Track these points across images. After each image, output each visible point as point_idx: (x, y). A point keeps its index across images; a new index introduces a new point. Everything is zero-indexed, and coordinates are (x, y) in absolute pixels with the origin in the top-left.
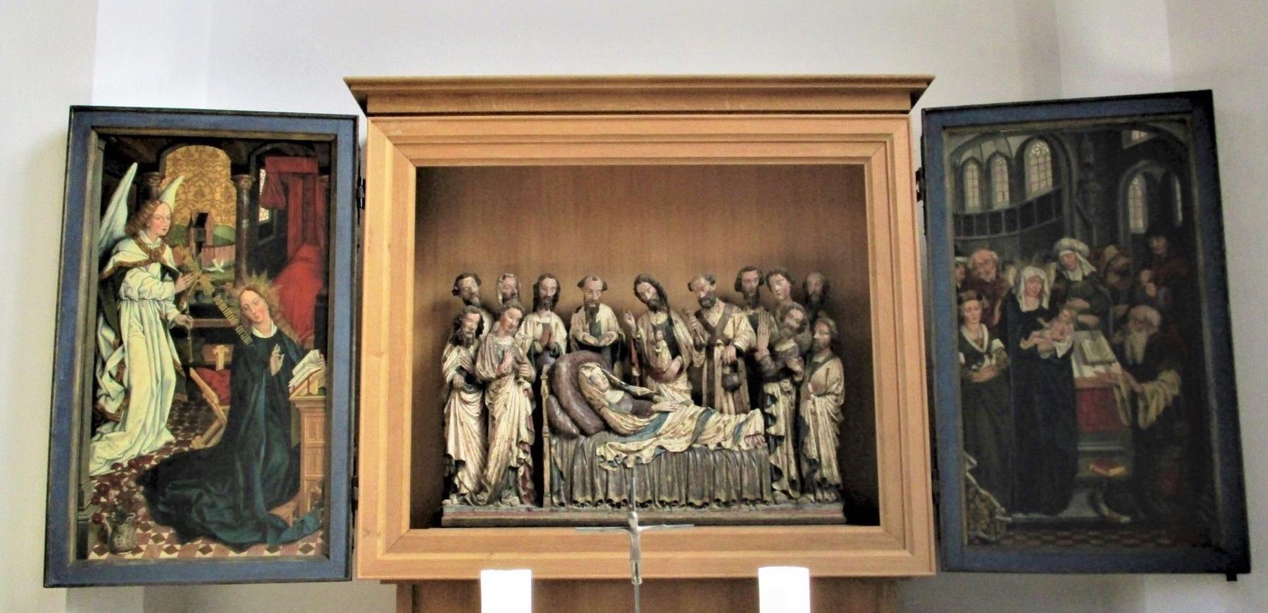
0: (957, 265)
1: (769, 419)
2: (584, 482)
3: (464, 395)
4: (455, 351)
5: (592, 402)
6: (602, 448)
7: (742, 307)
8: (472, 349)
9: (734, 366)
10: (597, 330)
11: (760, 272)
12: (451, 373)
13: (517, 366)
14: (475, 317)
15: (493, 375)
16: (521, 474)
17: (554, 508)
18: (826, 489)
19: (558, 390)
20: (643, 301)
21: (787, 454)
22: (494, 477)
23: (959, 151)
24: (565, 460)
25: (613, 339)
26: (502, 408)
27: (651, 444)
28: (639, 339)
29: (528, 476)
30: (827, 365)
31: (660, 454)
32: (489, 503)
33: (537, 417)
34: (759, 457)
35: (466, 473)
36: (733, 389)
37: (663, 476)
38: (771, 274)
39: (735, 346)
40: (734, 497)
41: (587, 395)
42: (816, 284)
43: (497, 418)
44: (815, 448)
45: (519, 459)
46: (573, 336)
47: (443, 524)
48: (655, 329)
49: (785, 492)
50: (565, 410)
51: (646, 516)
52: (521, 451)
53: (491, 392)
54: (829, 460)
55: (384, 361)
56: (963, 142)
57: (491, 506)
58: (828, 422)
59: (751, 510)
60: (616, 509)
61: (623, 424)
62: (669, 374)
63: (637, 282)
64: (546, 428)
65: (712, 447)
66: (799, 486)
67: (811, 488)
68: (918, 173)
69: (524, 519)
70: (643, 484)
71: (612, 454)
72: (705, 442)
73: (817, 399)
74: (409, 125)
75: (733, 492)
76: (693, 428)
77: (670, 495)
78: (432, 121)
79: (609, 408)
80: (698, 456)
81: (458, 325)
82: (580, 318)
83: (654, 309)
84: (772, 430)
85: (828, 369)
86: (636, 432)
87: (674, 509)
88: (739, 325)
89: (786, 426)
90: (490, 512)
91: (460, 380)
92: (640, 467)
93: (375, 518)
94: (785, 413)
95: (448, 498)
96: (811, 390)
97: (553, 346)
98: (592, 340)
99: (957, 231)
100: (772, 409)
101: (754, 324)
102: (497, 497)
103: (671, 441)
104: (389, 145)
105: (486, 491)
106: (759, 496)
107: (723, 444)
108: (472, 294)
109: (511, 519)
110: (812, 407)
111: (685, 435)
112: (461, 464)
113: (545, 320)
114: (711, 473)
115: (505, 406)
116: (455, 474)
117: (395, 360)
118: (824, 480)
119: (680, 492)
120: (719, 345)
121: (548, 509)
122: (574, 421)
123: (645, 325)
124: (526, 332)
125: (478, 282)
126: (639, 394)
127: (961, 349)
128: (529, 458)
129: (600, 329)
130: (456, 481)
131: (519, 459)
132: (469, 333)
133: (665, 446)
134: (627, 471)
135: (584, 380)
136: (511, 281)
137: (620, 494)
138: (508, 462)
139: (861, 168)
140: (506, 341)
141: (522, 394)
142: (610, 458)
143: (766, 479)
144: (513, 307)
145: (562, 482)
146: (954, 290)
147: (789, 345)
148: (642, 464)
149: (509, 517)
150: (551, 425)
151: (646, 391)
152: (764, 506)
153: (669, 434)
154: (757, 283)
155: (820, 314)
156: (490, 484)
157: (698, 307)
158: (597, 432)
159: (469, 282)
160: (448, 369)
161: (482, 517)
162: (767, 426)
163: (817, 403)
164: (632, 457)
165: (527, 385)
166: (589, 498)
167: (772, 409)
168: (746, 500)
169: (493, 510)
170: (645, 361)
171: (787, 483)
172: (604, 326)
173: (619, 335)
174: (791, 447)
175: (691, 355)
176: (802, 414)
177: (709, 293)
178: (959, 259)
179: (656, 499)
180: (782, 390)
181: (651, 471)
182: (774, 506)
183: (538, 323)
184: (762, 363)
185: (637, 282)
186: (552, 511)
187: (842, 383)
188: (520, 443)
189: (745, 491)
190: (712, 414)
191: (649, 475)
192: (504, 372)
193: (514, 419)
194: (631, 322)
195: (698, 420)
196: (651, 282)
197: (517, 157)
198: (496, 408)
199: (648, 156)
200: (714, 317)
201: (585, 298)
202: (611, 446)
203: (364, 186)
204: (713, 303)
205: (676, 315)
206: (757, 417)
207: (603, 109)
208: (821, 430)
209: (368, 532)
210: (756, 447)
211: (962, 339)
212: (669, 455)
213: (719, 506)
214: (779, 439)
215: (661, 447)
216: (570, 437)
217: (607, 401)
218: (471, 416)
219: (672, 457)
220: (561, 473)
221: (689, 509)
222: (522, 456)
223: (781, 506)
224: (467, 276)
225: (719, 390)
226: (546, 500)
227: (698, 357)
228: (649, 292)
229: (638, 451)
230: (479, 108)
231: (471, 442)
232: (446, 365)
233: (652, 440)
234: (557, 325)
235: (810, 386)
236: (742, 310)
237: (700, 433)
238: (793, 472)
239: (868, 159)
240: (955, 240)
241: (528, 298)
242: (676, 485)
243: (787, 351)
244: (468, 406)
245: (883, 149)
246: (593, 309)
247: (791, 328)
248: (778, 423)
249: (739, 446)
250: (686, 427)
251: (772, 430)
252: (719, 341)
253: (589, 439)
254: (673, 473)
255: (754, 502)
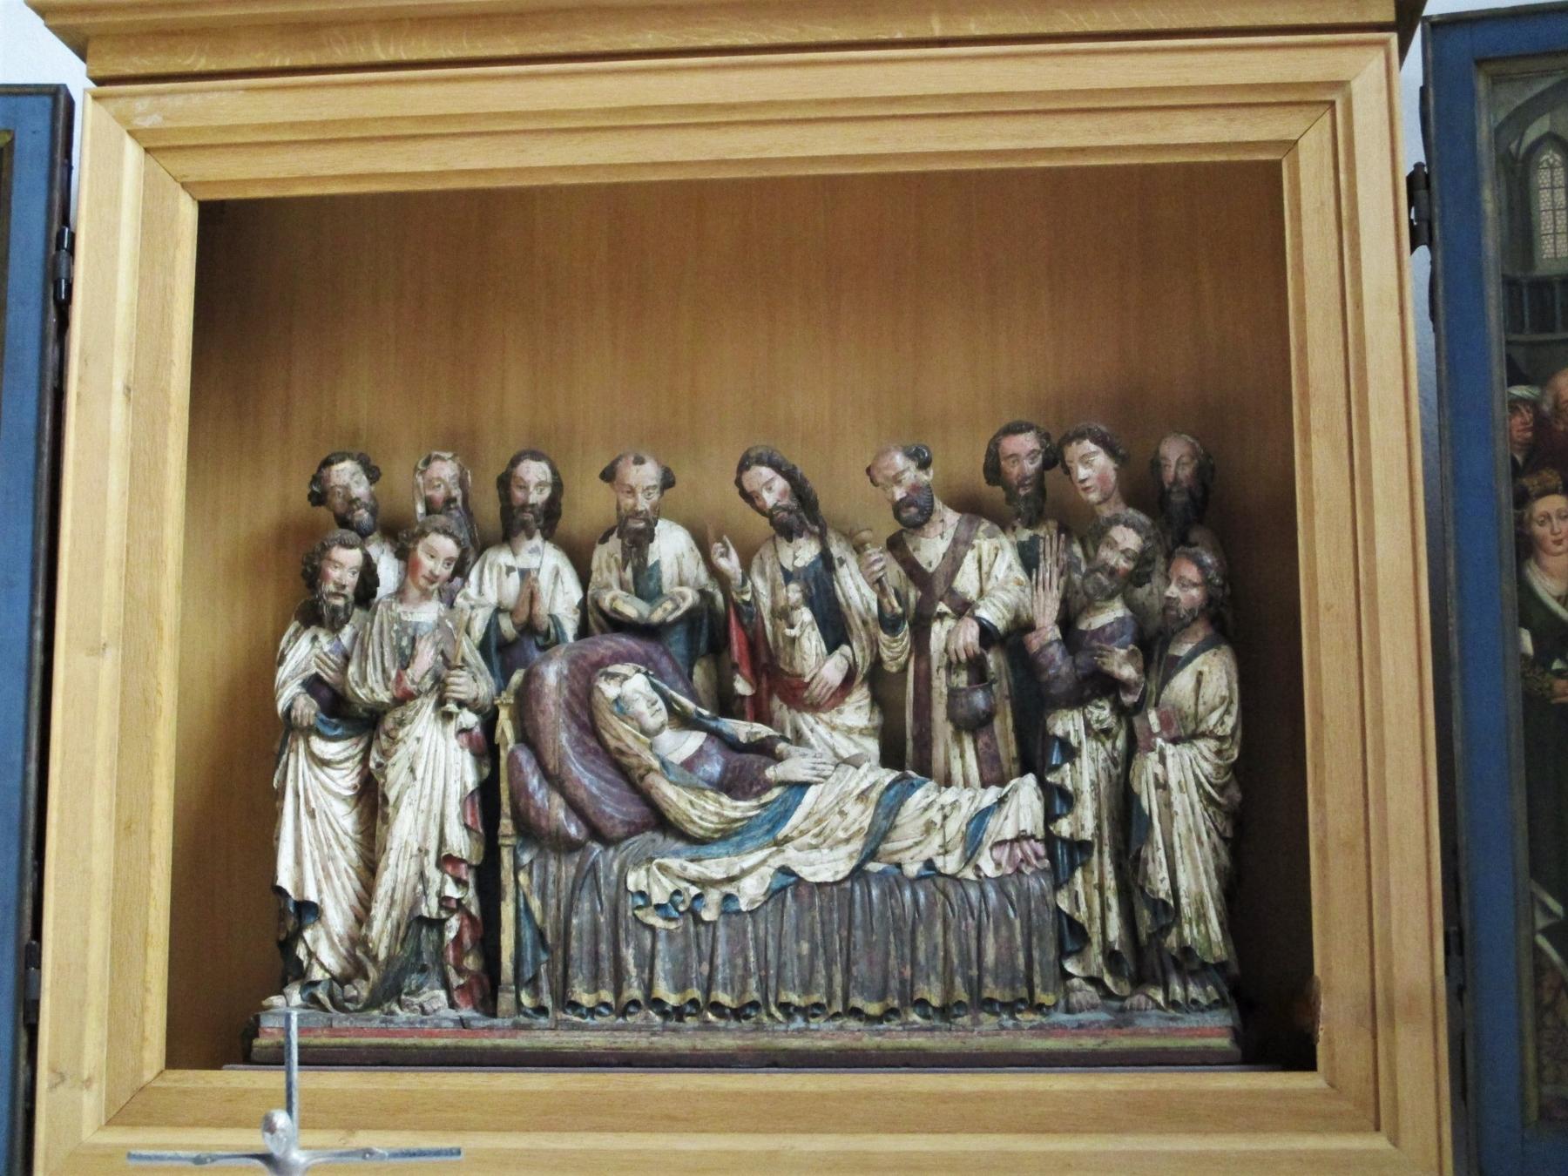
0: (1514, 405)
1: (1057, 800)
2: (596, 957)
3: (318, 745)
4: (304, 641)
5: (625, 760)
6: (643, 872)
7: (1004, 524)
8: (347, 633)
9: (976, 667)
10: (652, 584)
11: (1044, 436)
12: (289, 692)
13: (444, 672)
14: (352, 557)
15: (384, 696)
16: (450, 935)
17: (523, 1020)
18: (1193, 973)
19: (537, 731)
20: (761, 511)
21: (1101, 888)
22: (385, 941)
23: (1521, 117)
24: (553, 902)
25: (685, 606)
26: (404, 776)
27: (763, 862)
28: (748, 604)
29: (467, 939)
30: (1198, 663)
31: (783, 889)
32: (374, 1002)
33: (486, 798)
34: (1025, 895)
35: (322, 933)
36: (973, 725)
37: (789, 942)
38: (1068, 439)
39: (979, 620)
40: (962, 995)
41: (612, 743)
42: (1178, 462)
43: (392, 798)
44: (1164, 873)
45: (443, 900)
46: (592, 598)
47: (254, 1057)
48: (788, 577)
49: (1092, 980)
50: (554, 780)
51: (740, 1042)
52: (449, 880)
53: (383, 737)
54: (1201, 903)
55: (109, 667)
56: (1529, 94)
57: (376, 1012)
58: (1198, 807)
59: (1003, 1028)
60: (673, 1023)
61: (694, 814)
62: (817, 690)
63: (743, 467)
64: (506, 825)
65: (912, 869)
66: (1129, 966)
67: (1159, 973)
68: (1411, 179)
69: (445, 1048)
70: (740, 961)
71: (664, 888)
72: (896, 858)
73: (1170, 750)
74: (179, 101)
75: (958, 980)
76: (866, 824)
77: (807, 988)
78: (233, 89)
79: (663, 775)
80: (875, 892)
81: (313, 576)
82: (611, 555)
83: (788, 532)
84: (1064, 827)
85: (1200, 676)
86: (729, 835)
87: (814, 1023)
88: (991, 566)
89: (1098, 817)
90: (366, 1030)
91: (307, 709)
92: (734, 918)
93: (79, 1039)
94: (1095, 785)
95: (280, 992)
96: (1156, 728)
97: (544, 622)
98: (632, 608)
99: (1513, 321)
100: (1064, 776)
101: (1029, 558)
102: (390, 991)
103: (814, 855)
104: (132, 152)
105: (366, 977)
106: (1023, 992)
107: (939, 862)
108: (352, 502)
109: (416, 1047)
110: (1159, 769)
111: (848, 841)
112: (308, 911)
113: (526, 559)
114: (907, 937)
115: (412, 770)
116: (297, 935)
117: (135, 664)
118: (1187, 951)
119: (830, 979)
120: (942, 616)
121: (508, 1022)
122: (574, 807)
123: (768, 569)
124: (480, 592)
125: (373, 474)
126: (743, 739)
127: (1524, 622)
128: (470, 896)
129: (659, 579)
130: (301, 952)
131: (443, 900)
132: (336, 595)
133: (796, 869)
134: (702, 929)
135: (603, 706)
136: (445, 470)
137: (680, 987)
138: (415, 904)
139: (1271, 172)
140: (427, 613)
141: (454, 743)
142: (659, 897)
143: (1043, 952)
144: (437, 530)
145: (544, 957)
146: (1504, 468)
147: (1112, 613)
148: (739, 912)
149: (409, 1041)
150: (519, 817)
151: (763, 730)
152: (1038, 1018)
153: (808, 839)
154: (1038, 462)
155: (1195, 535)
156: (374, 959)
157: (894, 527)
158: (629, 835)
159: (346, 474)
160: (285, 683)
161: (346, 1041)
162: (1050, 817)
163: (1170, 761)
164: (714, 896)
165: (469, 719)
166: (607, 996)
167: (1064, 776)
168: (991, 1001)
169: (376, 1024)
170: (764, 659)
171: (1100, 959)
172: (668, 573)
173: (703, 593)
174: (1109, 868)
175: (874, 643)
176: (1136, 789)
177: (915, 488)
178: (1520, 391)
179: (771, 999)
180: (1088, 725)
181: (762, 933)
182: (1061, 1017)
183: (510, 570)
184: (1043, 661)
185: (743, 467)
186: (517, 1027)
187: (1235, 708)
188: (446, 861)
189: (988, 980)
190: (914, 787)
191: (756, 939)
192: (411, 687)
193: (431, 802)
194: (730, 564)
195: (878, 804)
196: (777, 467)
197: (429, 168)
198: (391, 774)
199: (741, 156)
200: (931, 550)
201: (618, 508)
202: (661, 868)
203: (71, 251)
204: (927, 514)
205: (843, 545)
206: (1026, 796)
207: (637, 46)
208: (1180, 826)
209: (60, 1077)
210: (1018, 871)
211: (1526, 593)
212: (803, 891)
213: (926, 1016)
214: (1079, 849)
215: (785, 871)
216: (568, 846)
217: (657, 756)
218: (337, 795)
219: (812, 895)
220: (540, 934)
221: (853, 1024)
222: (452, 891)
223: (1080, 1016)
224: (342, 460)
225: (942, 727)
226: (505, 1001)
227: (889, 648)
228: (770, 489)
229: (731, 880)
230: (340, 56)
231: (333, 859)
232: (283, 673)
233: (766, 852)
234: (557, 574)
235: (1153, 717)
236: (1003, 529)
237: (884, 836)
238: (1115, 930)
239: (1291, 146)
240: (1508, 343)
241: (489, 507)
242: (820, 964)
243: (1103, 628)
244: (327, 770)
245: (1327, 118)
246: (639, 532)
247: (1112, 572)
248: (1079, 810)
249: (977, 868)
250: (850, 819)
251: (1064, 827)
252: (942, 607)
253: (611, 852)
254: (813, 934)
255: (1011, 1008)
